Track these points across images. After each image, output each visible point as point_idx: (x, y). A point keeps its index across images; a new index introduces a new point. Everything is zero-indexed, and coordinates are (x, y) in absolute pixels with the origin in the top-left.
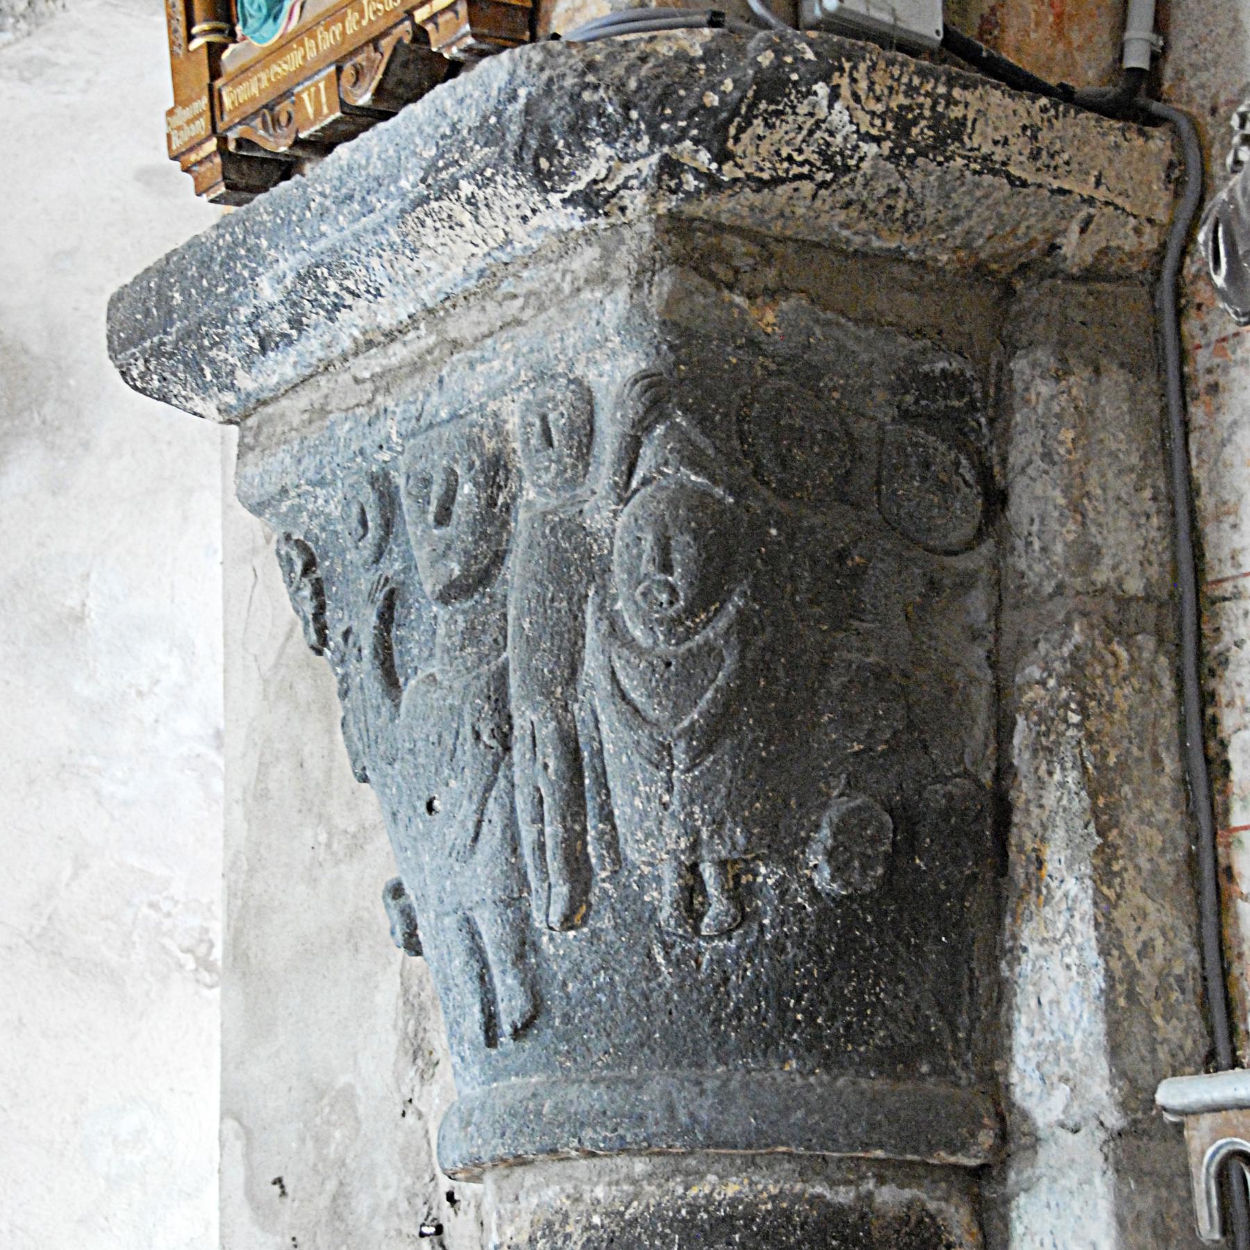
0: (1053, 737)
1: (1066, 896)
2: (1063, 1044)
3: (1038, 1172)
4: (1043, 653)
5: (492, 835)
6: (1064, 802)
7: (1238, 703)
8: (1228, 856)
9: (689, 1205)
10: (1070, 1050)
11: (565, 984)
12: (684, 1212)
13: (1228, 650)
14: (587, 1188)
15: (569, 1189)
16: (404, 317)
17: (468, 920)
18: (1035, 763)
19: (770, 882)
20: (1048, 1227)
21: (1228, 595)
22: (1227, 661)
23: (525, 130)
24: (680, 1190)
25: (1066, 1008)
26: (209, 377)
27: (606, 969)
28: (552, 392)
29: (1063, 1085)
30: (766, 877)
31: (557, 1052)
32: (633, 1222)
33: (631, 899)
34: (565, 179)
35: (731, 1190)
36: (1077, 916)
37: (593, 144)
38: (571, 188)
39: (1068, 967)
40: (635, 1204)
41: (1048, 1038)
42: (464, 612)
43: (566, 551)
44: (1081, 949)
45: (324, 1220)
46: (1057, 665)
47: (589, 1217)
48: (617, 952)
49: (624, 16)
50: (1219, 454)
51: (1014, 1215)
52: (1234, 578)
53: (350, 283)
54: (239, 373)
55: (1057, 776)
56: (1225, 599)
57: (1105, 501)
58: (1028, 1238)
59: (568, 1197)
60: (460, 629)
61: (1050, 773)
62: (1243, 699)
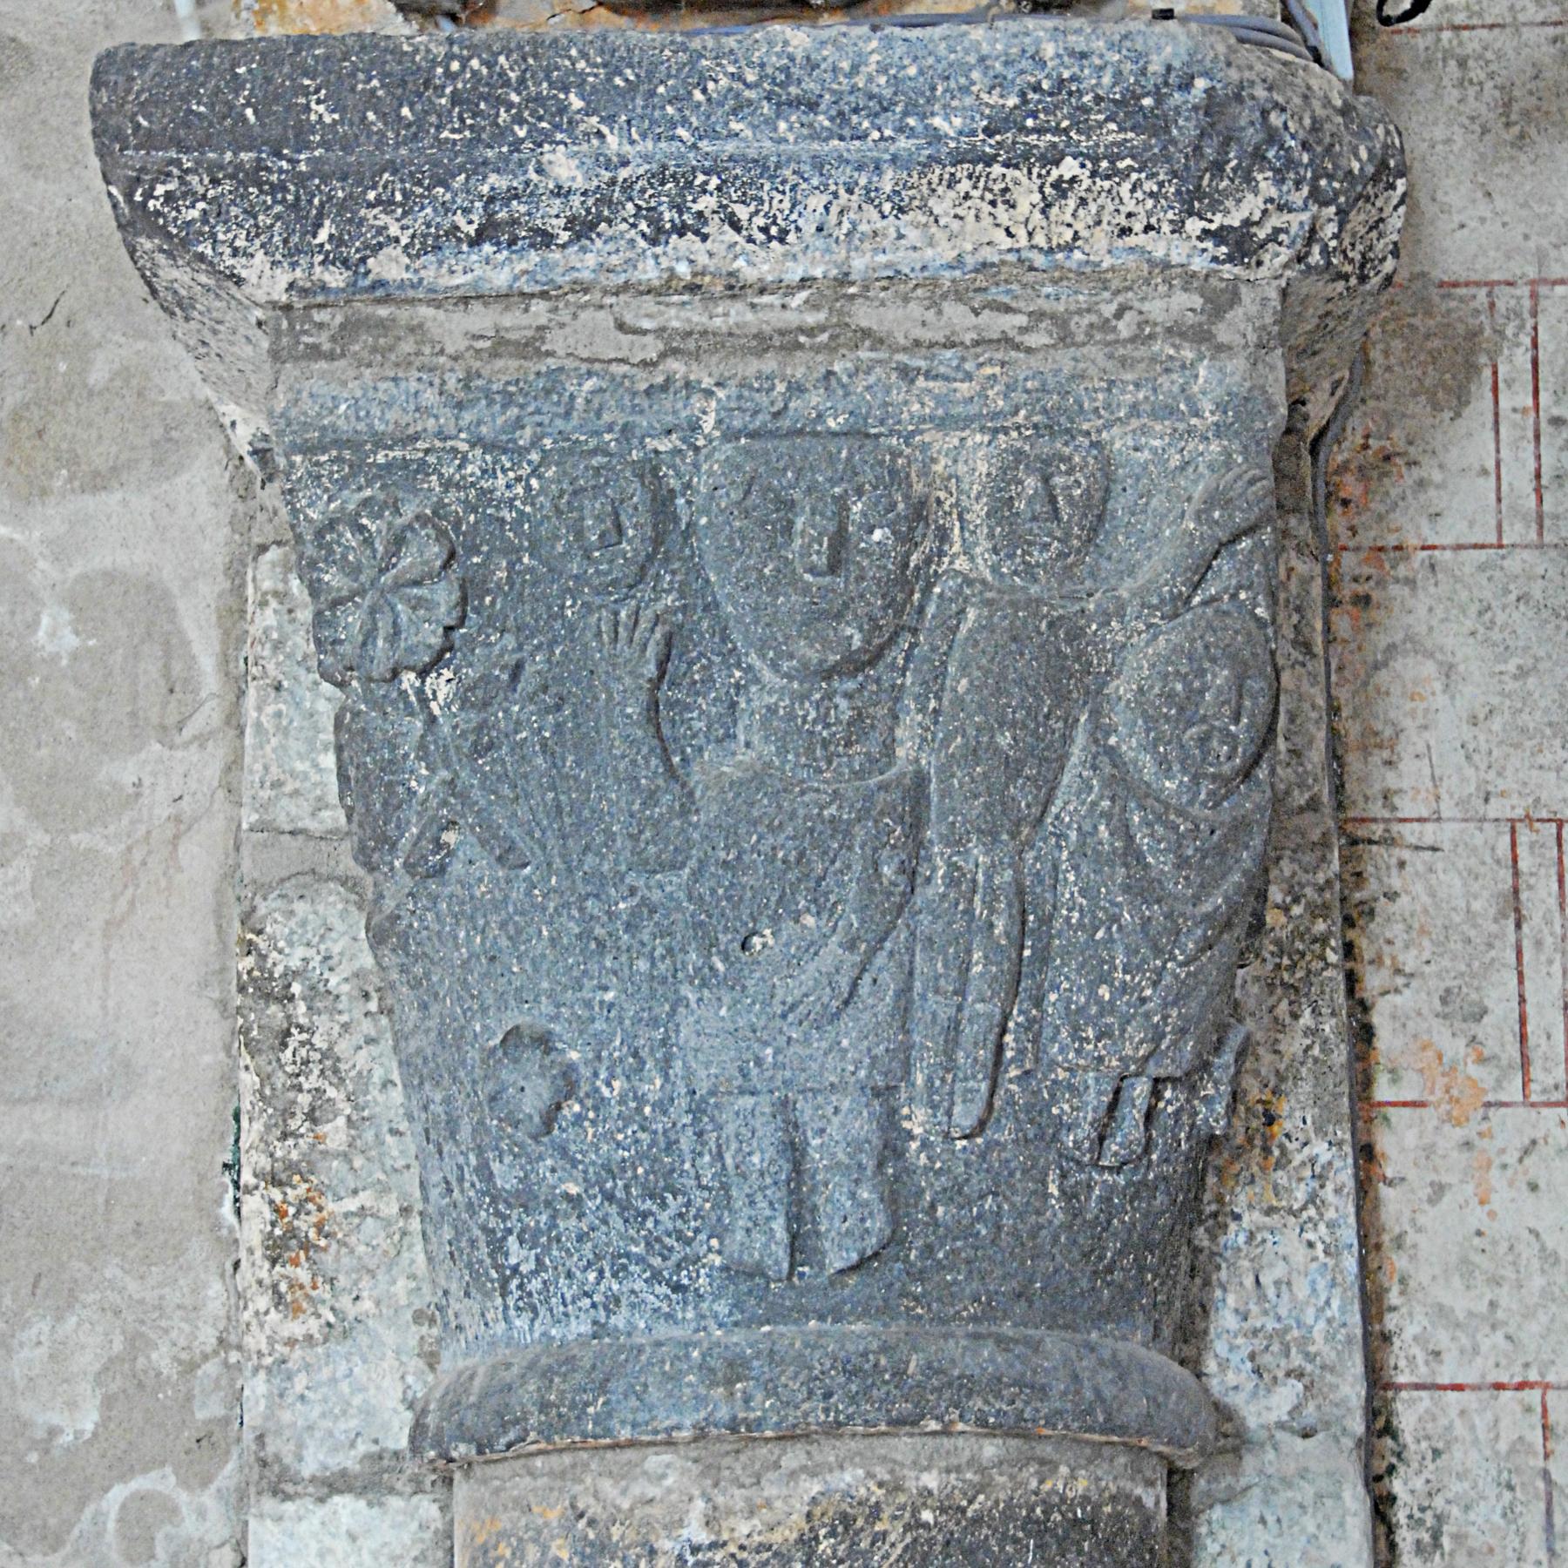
0: (1300, 974)
1: (1313, 1161)
2: (1295, 1333)
3: (1243, 1482)
4: (1287, 873)
5: (877, 1001)
6: (1316, 1051)
7: (1388, 962)
8: (1369, 1131)
9: (1044, 1502)
10: (1305, 1340)
11: (933, 1207)
12: (1038, 1511)
13: (1376, 900)
14: (913, 1474)
15: (882, 1473)
17: (785, 1103)
18: (1272, 1001)
19: (1170, 1109)
20: (1261, 1546)
21: (1376, 838)
22: (1372, 913)
23: (1202, 135)
24: (1034, 1484)
25: (1302, 1290)
27: (995, 1194)
28: (1067, 451)
29: (1293, 1381)
30: (1169, 1102)
31: (904, 1294)
32: (977, 1521)
33: (1037, 1109)
34: (1215, 206)
35: (1081, 1485)
36: (1330, 1187)
37: (1260, 177)
38: (1218, 220)
39: (1311, 1245)
40: (981, 1497)
41: (1271, 1325)
42: (848, 696)
43: (1066, 657)
44: (1331, 1225)
46: (1308, 891)
47: (915, 1512)
48: (1011, 1174)
49: (1255, 21)
50: (1369, 676)
51: (1203, 1530)
52: (1386, 821)
55: (1306, 1019)
56: (1370, 842)
58: (1227, 1558)
59: (880, 1485)
60: (845, 718)
61: (1295, 1016)
62: (1393, 958)
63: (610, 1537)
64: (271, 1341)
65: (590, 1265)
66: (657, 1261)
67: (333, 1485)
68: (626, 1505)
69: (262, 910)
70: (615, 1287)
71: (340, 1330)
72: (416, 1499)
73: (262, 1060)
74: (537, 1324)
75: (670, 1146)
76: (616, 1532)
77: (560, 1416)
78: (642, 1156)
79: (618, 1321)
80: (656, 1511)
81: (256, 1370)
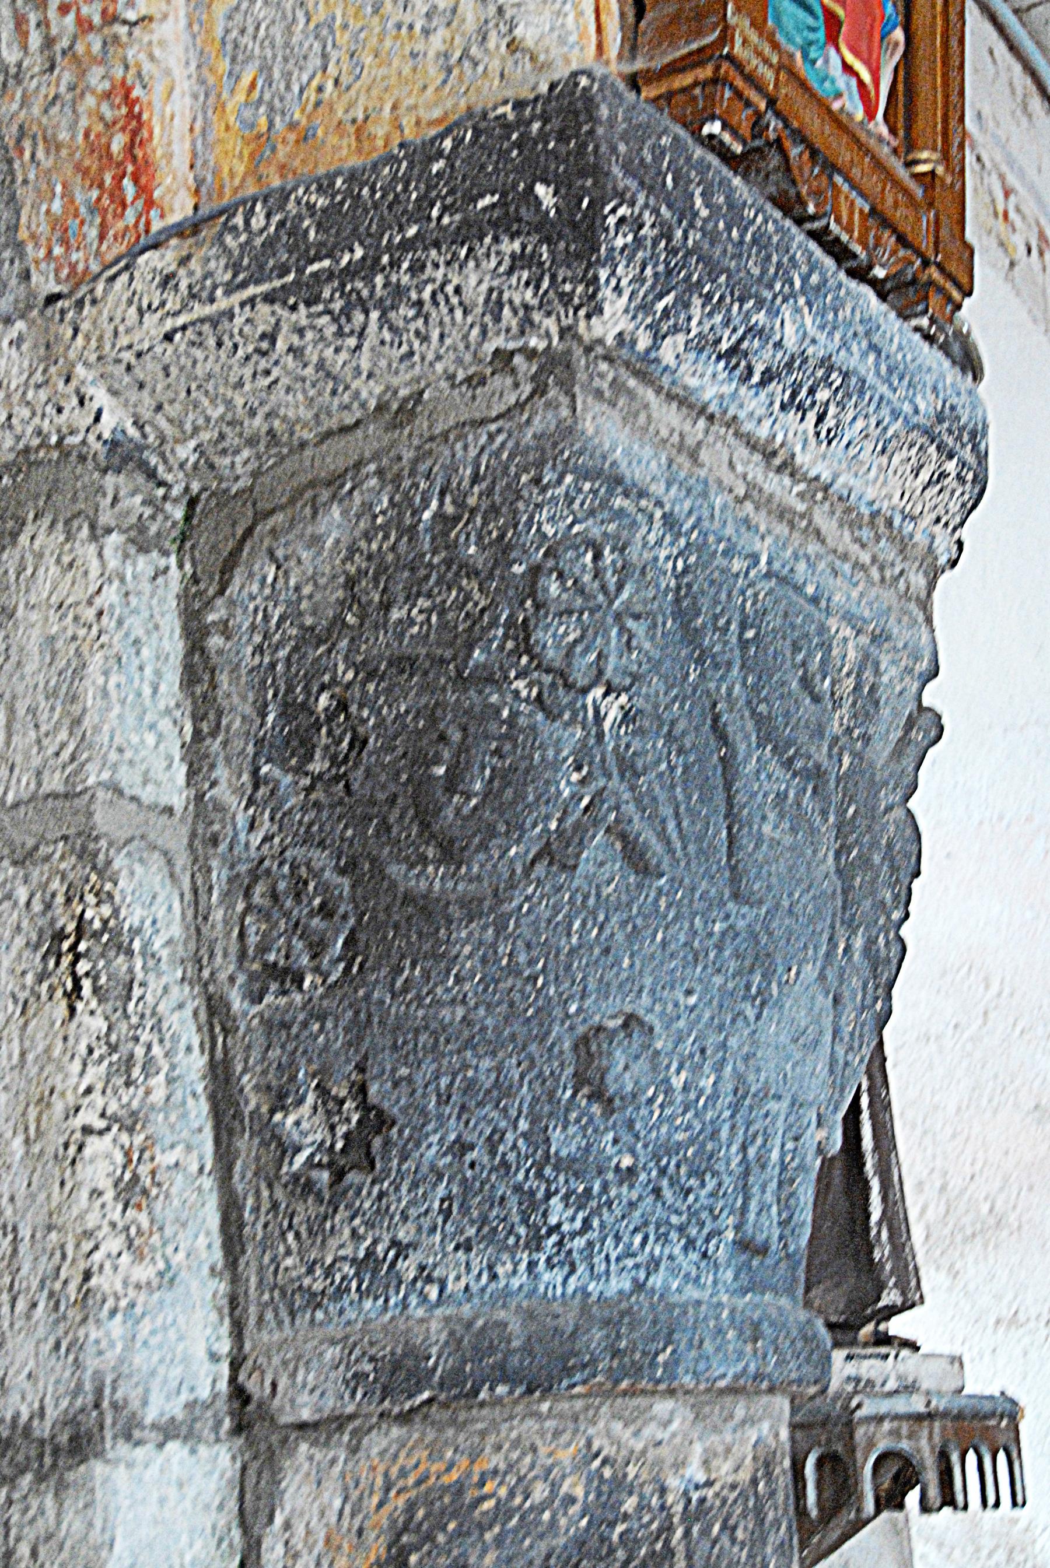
16: (812, 474)
26: (660, 306)
45: (208, 1168)
53: (832, 410)
54: (681, 338)
57: (44, 415)
63: (625, 1475)
64: (125, 1283)
65: (636, 1230)
66: (693, 1232)
67: (168, 1431)
68: (639, 1446)
69: (116, 865)
70: (657, 1252)
71: (167, 1278)
72: (217, 1447)
73: (109, 1007)
74: (572, 1280)
75: (714, 1135)
76: (632, 1471)
77: (633, 1363)
78: (692, 1141)
79: (656, 1281)
80: (664, 1451)
81: (113, 1312)
